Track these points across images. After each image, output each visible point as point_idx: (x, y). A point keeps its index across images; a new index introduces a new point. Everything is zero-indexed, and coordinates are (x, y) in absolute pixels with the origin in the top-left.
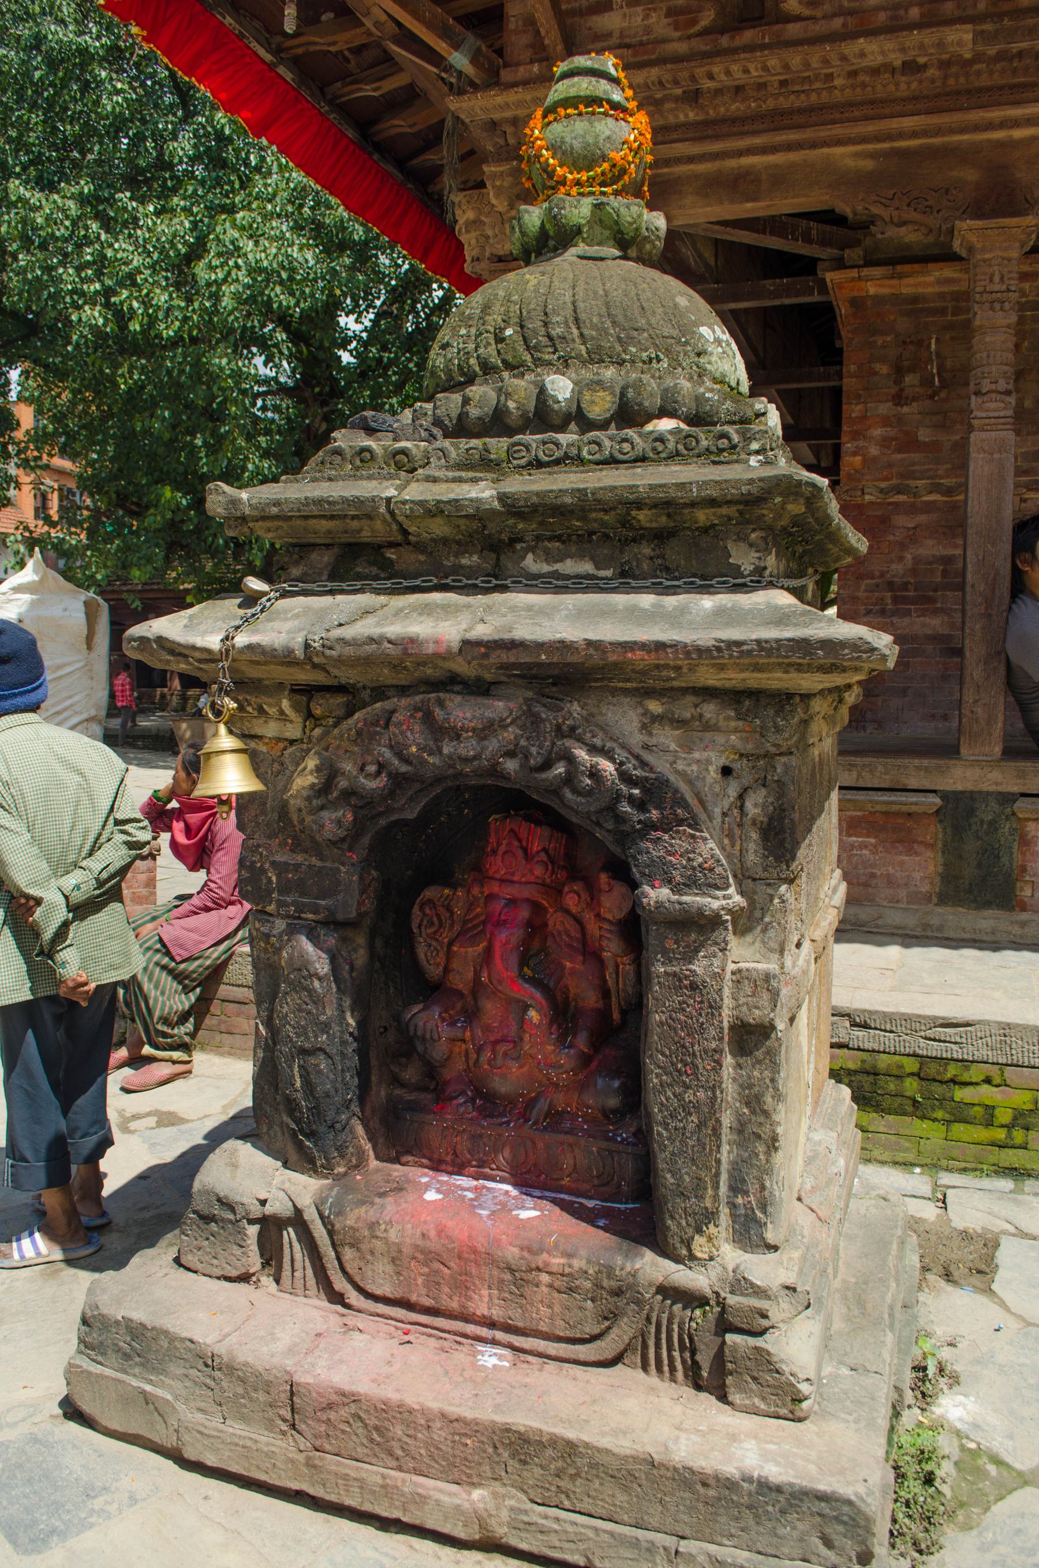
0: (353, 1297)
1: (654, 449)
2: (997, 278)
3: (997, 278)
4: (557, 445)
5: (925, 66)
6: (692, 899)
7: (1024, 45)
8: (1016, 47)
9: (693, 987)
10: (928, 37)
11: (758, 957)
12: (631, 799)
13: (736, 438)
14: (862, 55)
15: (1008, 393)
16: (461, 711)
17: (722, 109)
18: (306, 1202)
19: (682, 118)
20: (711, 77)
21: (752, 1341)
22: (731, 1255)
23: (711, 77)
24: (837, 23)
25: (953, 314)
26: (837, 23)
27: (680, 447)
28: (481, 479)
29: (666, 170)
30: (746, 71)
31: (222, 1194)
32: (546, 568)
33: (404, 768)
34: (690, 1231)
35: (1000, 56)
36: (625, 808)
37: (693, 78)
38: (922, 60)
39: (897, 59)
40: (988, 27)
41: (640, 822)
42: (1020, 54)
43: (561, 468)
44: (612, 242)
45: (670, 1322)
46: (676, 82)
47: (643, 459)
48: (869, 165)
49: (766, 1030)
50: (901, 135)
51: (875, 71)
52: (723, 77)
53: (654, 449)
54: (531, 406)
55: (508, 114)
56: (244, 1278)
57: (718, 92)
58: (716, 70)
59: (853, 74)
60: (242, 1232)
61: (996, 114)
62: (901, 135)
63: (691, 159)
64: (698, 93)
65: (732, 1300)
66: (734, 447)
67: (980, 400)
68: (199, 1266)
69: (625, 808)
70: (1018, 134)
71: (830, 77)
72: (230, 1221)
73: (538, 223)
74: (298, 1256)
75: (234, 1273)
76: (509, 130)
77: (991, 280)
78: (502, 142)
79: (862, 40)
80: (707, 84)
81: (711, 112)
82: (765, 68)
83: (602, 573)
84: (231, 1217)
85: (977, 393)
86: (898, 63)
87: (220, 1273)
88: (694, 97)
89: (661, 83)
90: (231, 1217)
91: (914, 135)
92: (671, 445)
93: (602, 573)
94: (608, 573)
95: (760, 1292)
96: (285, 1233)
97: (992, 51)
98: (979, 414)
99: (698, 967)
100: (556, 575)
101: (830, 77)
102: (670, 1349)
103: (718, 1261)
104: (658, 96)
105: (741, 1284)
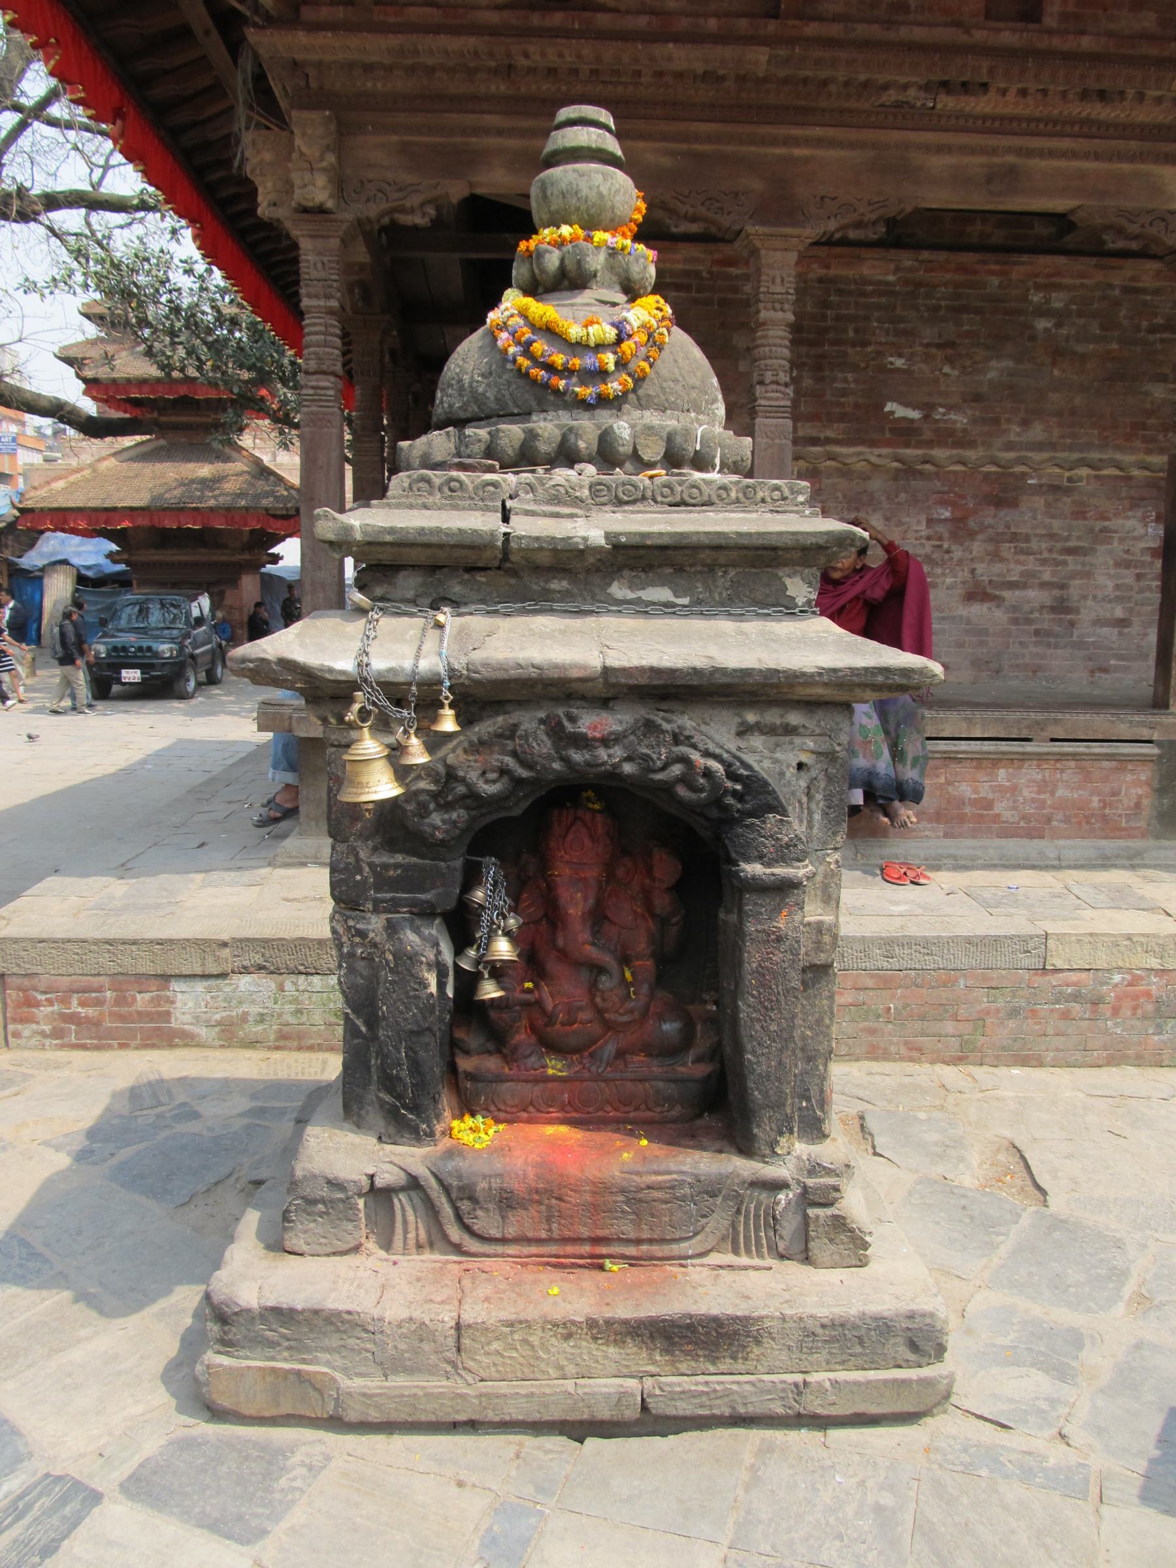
0: (473, 1245)
1: (719, 496)
2: (778, 280)
3: (778, 280)
4: (636, 487)
5: (723, 79)
6: (780, 871)
7: (808, 73)
8: (803, 73)
9: (779, 939)
10: (727, 52)
11: (819, 911)
12: (735, 793)
13: (787, 492)
14: (670, 59)
15: (786, 385)
16: (589, 722)
17: (534, 87)
18: (421, 1171)
19: (493, 88)
20: (526, 55)
21: (829, 1211)
22: (801, 1148)
23: (526, 55)
24: (642, 22)
25: (698, 292)
26: (642, 22)
27: (741, 495)
28: (576, 516)
29: (474, 140)
30: (561, 55)
31: (331, 1176)
32: (631, 595)
33: (524, 773)
34: (773, 1134)
35: (786, 80)
36: (730, 800)
37: (509, 55)
38: (721, 72)
39: (699, 67)
40: (782, 52)
41: (738, 811)
42: (805, 81)
43: (639, 506)
44: (618, 288)
45: (757, 1208)
46: (491, 55)
47: (709, 503)
48: (666, 162)
49: (826, 968)
50: (697, 138)
51: (679, 75)
52: (537, 57)
53: (719, 496)
54: (595, 447)
55: (313, 57)
56: (356, 1249)
57: (532, 70)
58: (531, 49)
59: (660, 74)
60: (354, 1207)
61: (782, 131)
62: (697, 138)
63: (500, 132)
64: (510, 67)
65: (810, 1182)
66: (784, 499)
67: (763, 389)
68: (305, 1248)
69: (730, 800)
70: (797, 152)
71: (638, 74)
72: (341, 1200)
73: (557, 263)
74: (411, 1217)
75: (346, 1247)
76: (312, 73)
77: (773, 282)
78: (302, 84)
79: (671, 45)
80: (522, 62)
81: (523, 89)
82: (579, 57)
83: (680, 601)
84: (342, 1196)
85: (761, 383)
86: (700, 71)
87: (329, 1250)
88: (508, 71)
89: (476, 53)
90: (342, 1196)
91: (709, 139)
92: (733, 495)
93: (680, 601)
94: (685, 601)
95: (830, 1172)
96: (396, 1201)
97: (782, 73)
98: (763, 402)
99: (781, 923)
100: (638, 601)
101: (638, 74)
102: (757, 1229)
103: (791, 1158)
104: (471, 65)
105: (815, 1169)
